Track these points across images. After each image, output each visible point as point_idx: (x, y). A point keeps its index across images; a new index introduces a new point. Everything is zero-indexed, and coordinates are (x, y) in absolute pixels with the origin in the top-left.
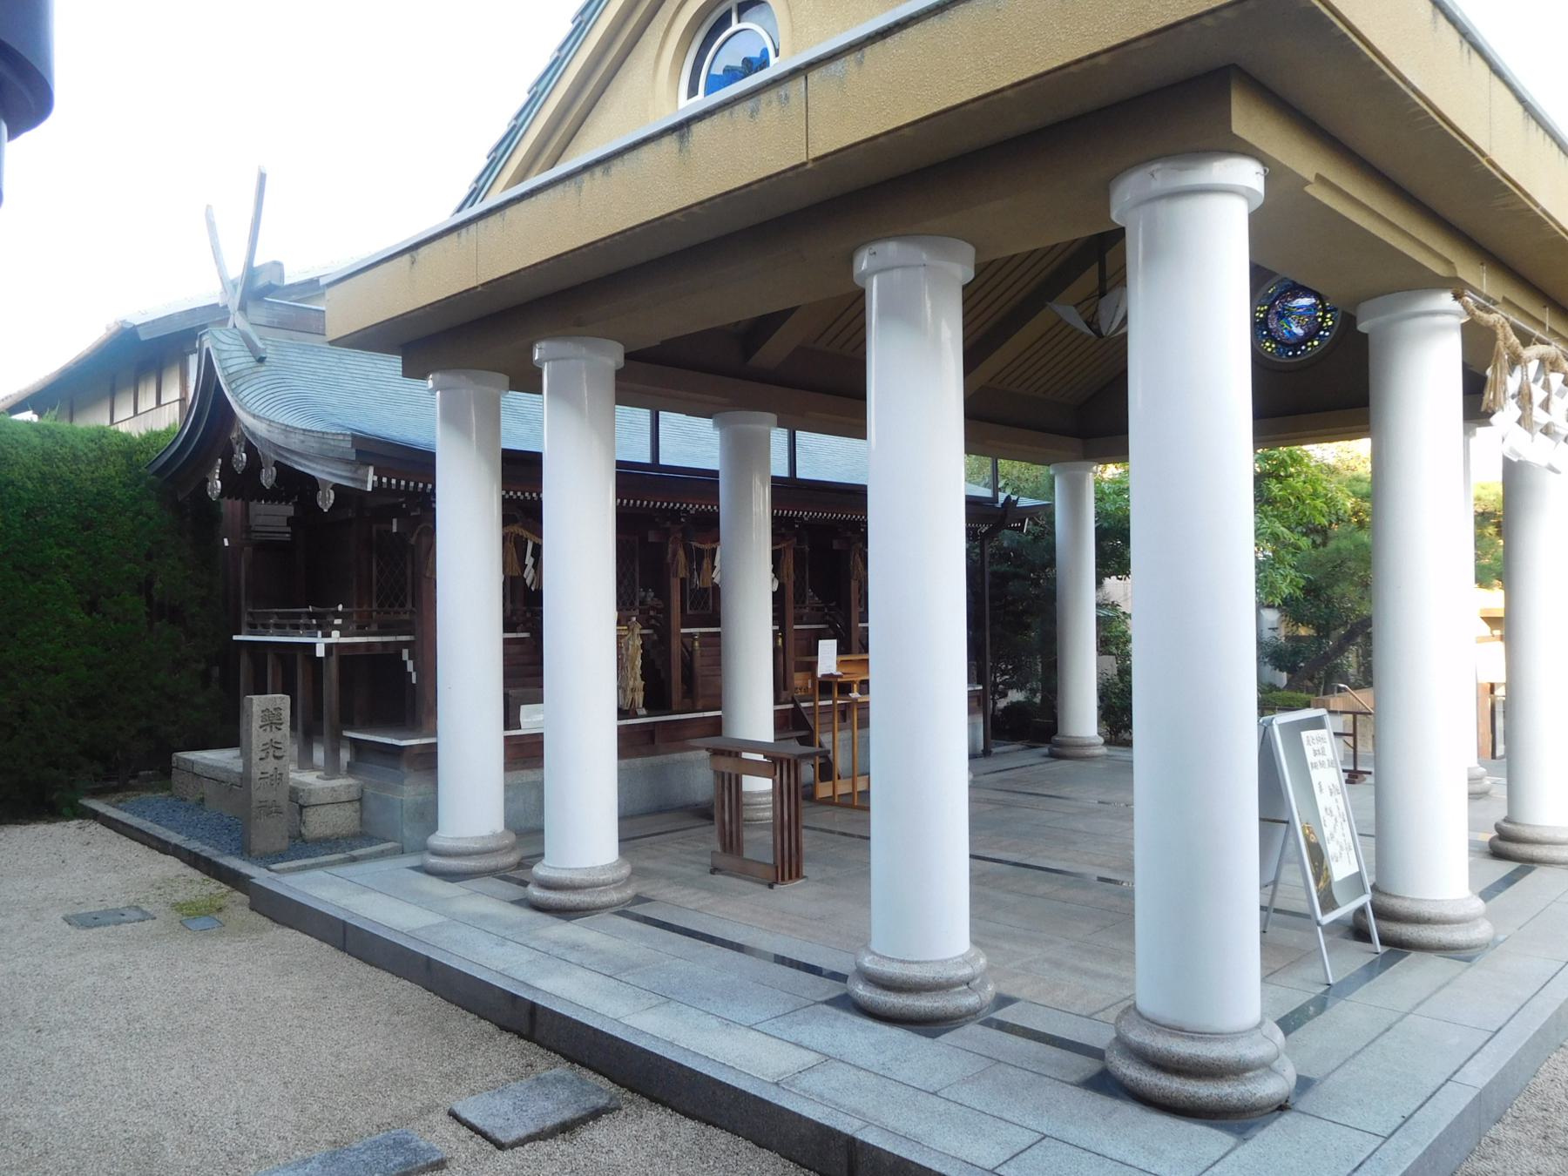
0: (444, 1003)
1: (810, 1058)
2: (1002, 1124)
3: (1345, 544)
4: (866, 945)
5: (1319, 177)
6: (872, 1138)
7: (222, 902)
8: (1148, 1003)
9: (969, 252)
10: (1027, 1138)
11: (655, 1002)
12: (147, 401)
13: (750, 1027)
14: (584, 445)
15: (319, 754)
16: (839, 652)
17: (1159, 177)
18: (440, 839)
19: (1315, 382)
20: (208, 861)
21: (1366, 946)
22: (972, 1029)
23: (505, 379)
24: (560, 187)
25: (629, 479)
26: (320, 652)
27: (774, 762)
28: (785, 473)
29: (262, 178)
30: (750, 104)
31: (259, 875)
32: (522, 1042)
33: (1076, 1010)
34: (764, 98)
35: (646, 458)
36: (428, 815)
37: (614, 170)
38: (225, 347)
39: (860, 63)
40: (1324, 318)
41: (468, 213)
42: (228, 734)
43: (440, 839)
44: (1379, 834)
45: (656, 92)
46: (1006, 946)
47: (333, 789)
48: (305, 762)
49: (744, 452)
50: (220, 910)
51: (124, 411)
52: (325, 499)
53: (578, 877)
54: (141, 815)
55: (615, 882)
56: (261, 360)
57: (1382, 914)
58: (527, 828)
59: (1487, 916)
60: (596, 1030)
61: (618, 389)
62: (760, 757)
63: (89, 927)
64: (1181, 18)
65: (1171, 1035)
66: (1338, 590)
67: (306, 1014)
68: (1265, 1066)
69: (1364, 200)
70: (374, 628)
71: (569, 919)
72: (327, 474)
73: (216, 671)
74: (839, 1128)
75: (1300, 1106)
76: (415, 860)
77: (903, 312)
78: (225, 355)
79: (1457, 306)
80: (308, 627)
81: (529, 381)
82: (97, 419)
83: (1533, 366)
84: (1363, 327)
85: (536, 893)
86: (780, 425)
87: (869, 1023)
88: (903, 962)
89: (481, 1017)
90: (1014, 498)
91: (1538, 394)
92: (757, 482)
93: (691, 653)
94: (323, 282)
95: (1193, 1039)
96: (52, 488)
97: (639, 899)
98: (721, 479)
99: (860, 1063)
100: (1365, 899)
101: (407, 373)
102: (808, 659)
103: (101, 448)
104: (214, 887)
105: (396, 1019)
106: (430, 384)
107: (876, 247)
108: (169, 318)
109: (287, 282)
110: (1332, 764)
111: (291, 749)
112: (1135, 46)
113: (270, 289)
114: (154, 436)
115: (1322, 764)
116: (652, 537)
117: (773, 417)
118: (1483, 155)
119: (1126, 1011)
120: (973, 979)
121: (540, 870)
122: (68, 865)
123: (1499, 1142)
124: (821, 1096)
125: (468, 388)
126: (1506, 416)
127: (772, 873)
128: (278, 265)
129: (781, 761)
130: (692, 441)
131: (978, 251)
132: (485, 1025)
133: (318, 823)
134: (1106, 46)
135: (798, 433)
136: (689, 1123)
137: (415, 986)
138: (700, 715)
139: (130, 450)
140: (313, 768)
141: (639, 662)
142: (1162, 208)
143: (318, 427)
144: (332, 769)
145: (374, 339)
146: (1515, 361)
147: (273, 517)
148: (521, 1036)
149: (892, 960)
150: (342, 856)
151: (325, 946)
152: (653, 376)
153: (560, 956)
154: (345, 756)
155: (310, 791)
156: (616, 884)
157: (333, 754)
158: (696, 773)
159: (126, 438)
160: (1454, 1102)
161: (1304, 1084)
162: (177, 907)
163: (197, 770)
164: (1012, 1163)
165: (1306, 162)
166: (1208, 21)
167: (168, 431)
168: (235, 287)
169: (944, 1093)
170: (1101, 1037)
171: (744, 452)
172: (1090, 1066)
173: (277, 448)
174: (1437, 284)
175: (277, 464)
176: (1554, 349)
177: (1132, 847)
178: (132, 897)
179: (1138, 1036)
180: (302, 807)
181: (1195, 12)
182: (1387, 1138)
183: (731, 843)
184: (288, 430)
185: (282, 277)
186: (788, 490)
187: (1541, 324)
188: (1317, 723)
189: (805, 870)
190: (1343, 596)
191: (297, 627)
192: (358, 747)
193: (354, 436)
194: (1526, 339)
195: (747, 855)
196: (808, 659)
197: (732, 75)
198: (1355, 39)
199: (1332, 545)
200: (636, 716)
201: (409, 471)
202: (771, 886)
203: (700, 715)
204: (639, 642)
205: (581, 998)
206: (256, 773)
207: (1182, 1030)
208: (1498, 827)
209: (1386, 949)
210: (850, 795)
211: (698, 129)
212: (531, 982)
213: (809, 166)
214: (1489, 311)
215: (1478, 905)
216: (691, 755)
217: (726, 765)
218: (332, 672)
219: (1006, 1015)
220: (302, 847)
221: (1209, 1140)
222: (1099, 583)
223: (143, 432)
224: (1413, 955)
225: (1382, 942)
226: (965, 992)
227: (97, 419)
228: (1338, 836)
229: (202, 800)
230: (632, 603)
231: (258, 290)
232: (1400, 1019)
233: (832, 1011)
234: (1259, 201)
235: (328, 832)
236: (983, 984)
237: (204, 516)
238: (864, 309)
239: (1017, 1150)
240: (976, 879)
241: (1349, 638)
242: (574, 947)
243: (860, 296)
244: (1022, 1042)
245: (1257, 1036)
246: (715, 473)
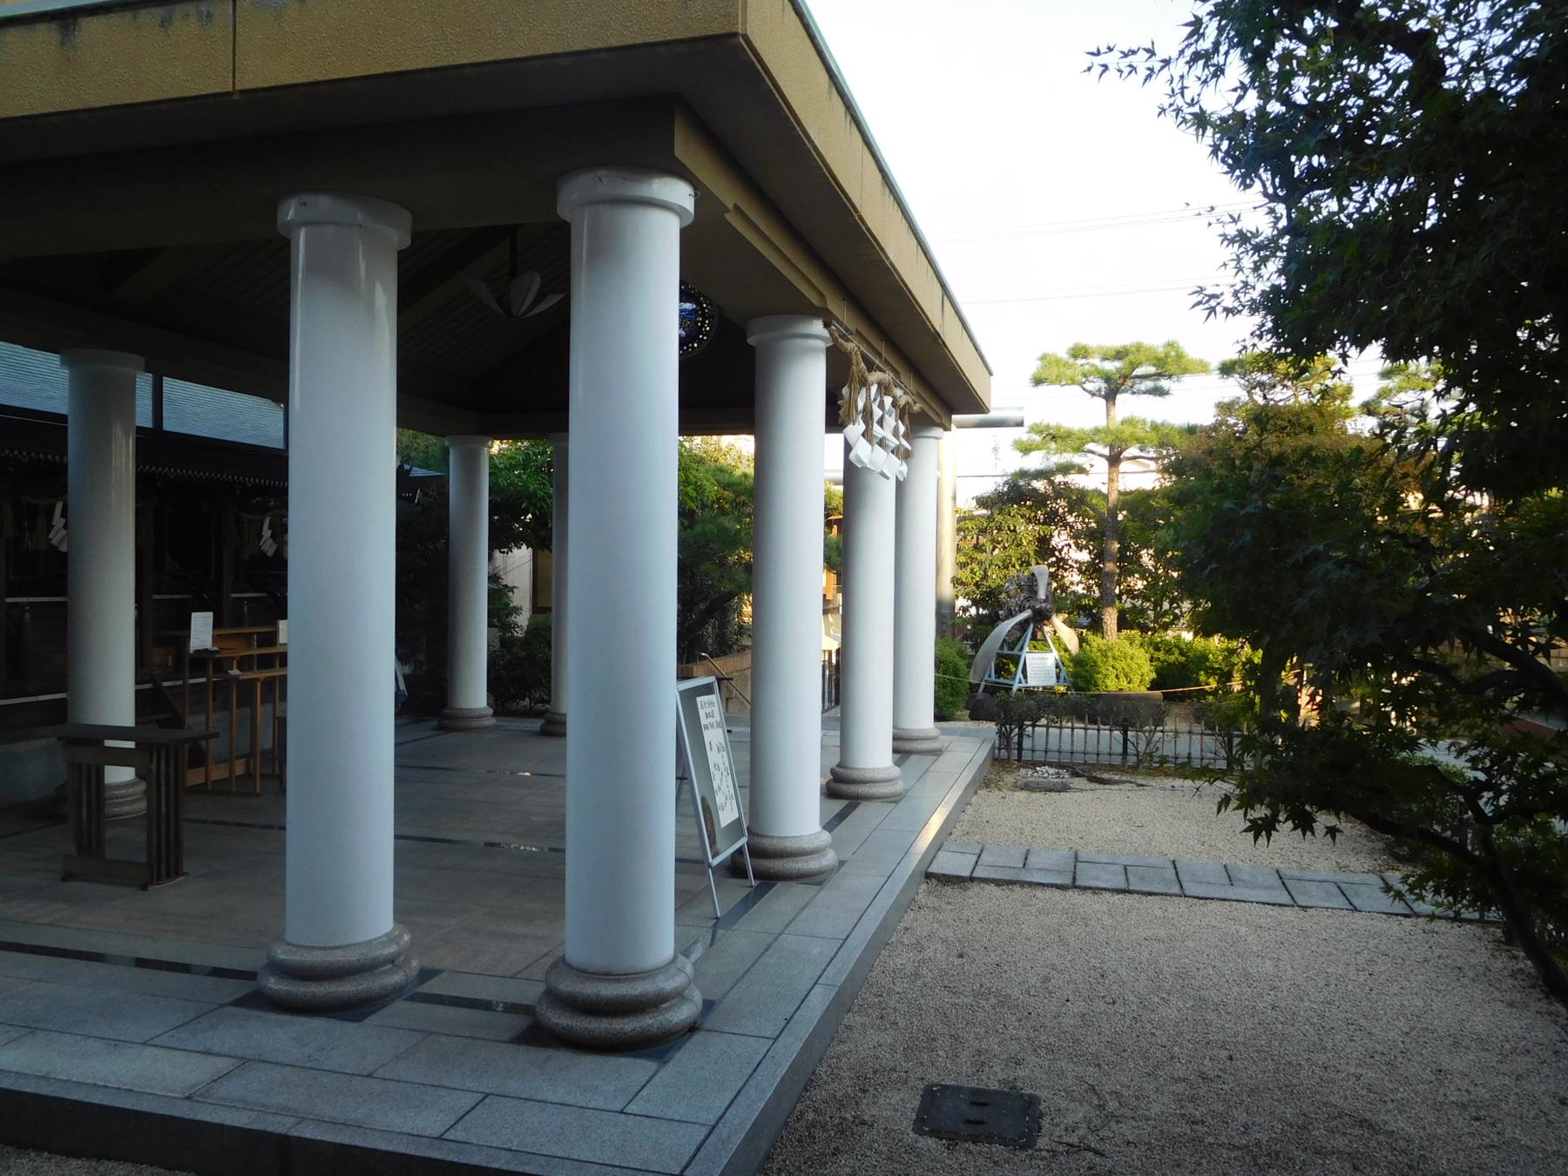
1: (224, 1064)
2: (444, 1092)
3: (708, 527)
4: (279, 937)
6: (308, 1132)
8: (576, 952)
10: (468, 1101)
13: (145, 1044)
16: (216, 625)
17: (603, 183)
19: (723, 385)
22: (400, 1006)
28: (149, 424)
40: (703, 323)
44: (755, 781)
49: (102, 398)
57: (757, 852)
59: (833, 846)
62: (130, 745)
64: (560, 50)
66: (703, 568)
68: (678, 995)
69: (762, 227)
74: (270, 1129)
75: (706, 1026)
77: (333, 270)
79: (825, 333)
83: (874, 388)
84: (751, 341)
88: (325, 948)
90: (407, 467)
91: (877, 413)
92: (118, 431)
95: (619, 981)
99: (282, 1059)
100: (743, 841)
102: (176, 633)
107: (308, 198)
110: (719, 725)
117: (141, 360)
119: (555, 965)
120: (399, 954)
123: (849, 1028)
124: (245, 1102)
126: (855, 429)
135: (168, 382)
136: (74, 1163)
146: (864, 383)
149: (312, 948)
160: (819, 1001)
161: (709, 1006)
164: (459, 1126)
165: (728, 194)
169: (380, 1073)
170: (530, 993)
171: (102, 398)
172: (519, 1023)
176: (887, 376)
177: (564, 806)
179: (568, 986)
181: (652, 39)
182: (776, 1039)
186: (157, 446)
187: (879, 355)
190: (707, 574)
194: (871, 367)
195: (110, 854)
196: (176, 633)
199: (698, 528)
207: (608, 974)
208: (833, 772)
210: (206, 784)
213: (235, 97)
214: (848, 340)
215: (826, 837)
216: (21, 747)
219: (433, 987)
221: (634, 1069)
222: (491, 557)
224: (779, 884)
228: (724, 788)
233: (243, 1011)
234: (690, 220)
239: (462, 1112)
241: (709, 612)
243: (282, 249)
244: (451, 1011)
245: (673, 970)
246: (63, 418)
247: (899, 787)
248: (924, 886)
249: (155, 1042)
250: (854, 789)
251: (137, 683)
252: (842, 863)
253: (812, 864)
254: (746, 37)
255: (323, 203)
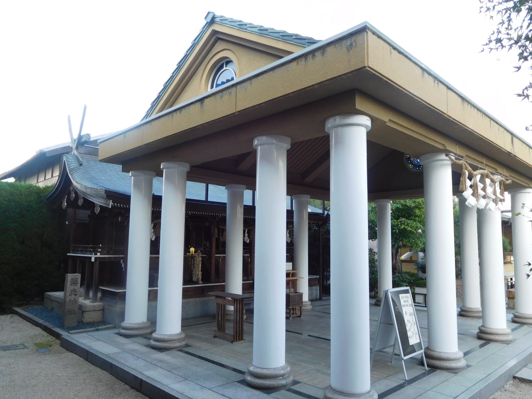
0: (115, 379)
5: (390, 120)
7: (52, 343)
9: (289, 140)
11: (181, 380)
12: (49, 176)
14: (176, 194)
15: (91, 294)
17: (338, 120)
18: (125, 324)
20: (50, 329)
21: (421, 367)
22: (283, 392)
23: (155, 173)
24: (167, 116)
25: (191, 206)
26: (93, 260)
27: (235, 301)
29: (85, 108)
30: (220, 94)
31: (65, 334)
32: (137, 393)
33: (319, 386)
34: (224, 92)
35: (203, 199)
36: (122, 316)
37: (182, 112)
38: (70, 160)
39: (251, 84)
41: (149, 119)
42: (61, 287)
43: (125, 324)
44: (428, 328)
45: (200, 87)
46: (303, 364)
47: (94, 306)
48: (87, 297)
49: (236, 197)
50: (50, 346)
51: (41, 179)
52: (97, 210)
53: (166, 338)
54: (32, 313)
55: (178, 339)
56: (81, 165)
57: (428, 356)
58: (153, 319)
60: (159, 389)
61: (188, 176)
63: (6, 350)
64: (336, 76)
65: (339, 394)
67: (69, 381)
70: (112, 252)
71: (162, 352)
72: (98, 202)
73: (62, 265)
76: (116, 331)
77: (268, 159)
78: (70, 163)
79: (447, 158)
80: (90, 251)
81: (160, 174)
82: (33, 182)
83: (478, 177)
85: (153, 342)
86: (248, 188)
87: (249, 389)
89: (126, 384)
92: (238, 207)
93: (219, 263)
94: (98, 141)
95: (346, 396)
96: (12, 204)
97: (187, 346)
98: (227, 206)
101: (124, 170)
103: (30, 191)
104: (51, 338)
105: (98, 384)
106: (130, 174)
107: (259, 138)
108: (57, 150)
109: (91, 140)
111: (82, 290)
112: (324, 83)
113: (86, 142)
114: (47, 188)
115: (407, 305)
116: (207, 224)
117: (245, 186)
118: (445, 114)
121: (154, 335)
122: (9, 328)
125: (143, 177)
127: (233, 339)
128: (88, 135)
129: (237, 300)
130: (218, 194)
131: (292, 140)
132: (127, 387)
133: (88, 318)
134: (316, 83)
137: (107, 373)
138: (220, 284)
139: (39, 192)
140: (89, 299)
141: (200, 266)
142: (340, 129)
143: (95, 187)
144: (95, 299)
145: (112, 160)
147: (83, 214)
148: (137, 391)
150: (94, 329)
151: (81, 359)
152: (200, 172)
153: (154, 364)
154: (99, 295)
155: (86, 307)
156: (179, 340)
157: (95, 294)
158: (212, 302)
159: (38, 188)
162: (36, 344)
163: (52, 298)
165: (385, 116)
166: (343, 77)
167: (52, 186)
168: (75, 141)
171: (236, 197)
173: (84, 193)
174: (439, 151)
175: (84, 198)
178: (23, 340)
180: (83, 312)
181: (340, 74)
183: (221, 328)
184: (86, 188)
185: (90, 138)
188: (406, 292)
189: (244, 338)
191: (86, 251)
192: (104, 292)
193: (105, 190)
194: (475, 168)
197: (223, 83)
198: (390, 82)
200: (198, 284)
201: (122, 201)
202: (232, 343)
203: (220, 284)
204: (200, 259)
205: (157, 378)
206: (68, 300)
208: (479, 329)
209: (430, 369)
211: (206, 101)
212: (143, 372)
214: (461, 160)
217: (220, 301)
218: (97, 267)
219: (296, 388)
220: (82, 325)
223: (44, 186)
224: (438, 371)
225: (428, 366)
226: (281, 379)
227: (33, 182)
228: (412, 329)
229: (53, 308)
230: (201, 246)
231: (82, 143)
232: (425, 392)
233: (239, 384)
234: (370, 129)
235: (91, 320)
236: (289, 376)
237: (62, 213)
238: (329, 141)
240: (287, 339)
242: (161, 361)
243: (255, 152)
245: (368, 395)
246: (225, 204)
247: (510, 337)
248: (511, 382)
249: (212, 389)
250: (491, 337)
251: (243, 281)
252: (468, 366)
253: (453, 365)
254: (369, 67)
255: (264, 139)
